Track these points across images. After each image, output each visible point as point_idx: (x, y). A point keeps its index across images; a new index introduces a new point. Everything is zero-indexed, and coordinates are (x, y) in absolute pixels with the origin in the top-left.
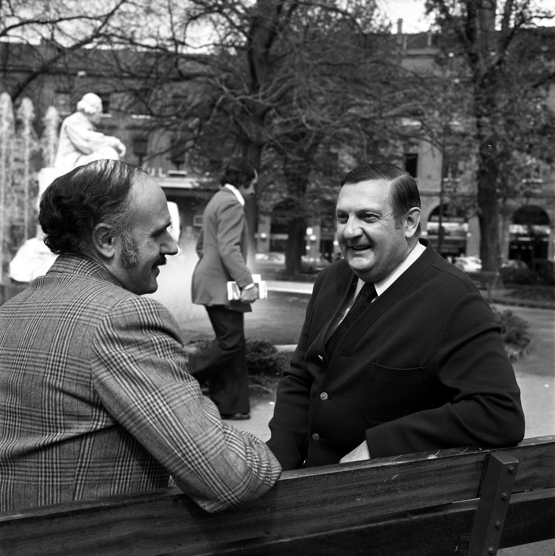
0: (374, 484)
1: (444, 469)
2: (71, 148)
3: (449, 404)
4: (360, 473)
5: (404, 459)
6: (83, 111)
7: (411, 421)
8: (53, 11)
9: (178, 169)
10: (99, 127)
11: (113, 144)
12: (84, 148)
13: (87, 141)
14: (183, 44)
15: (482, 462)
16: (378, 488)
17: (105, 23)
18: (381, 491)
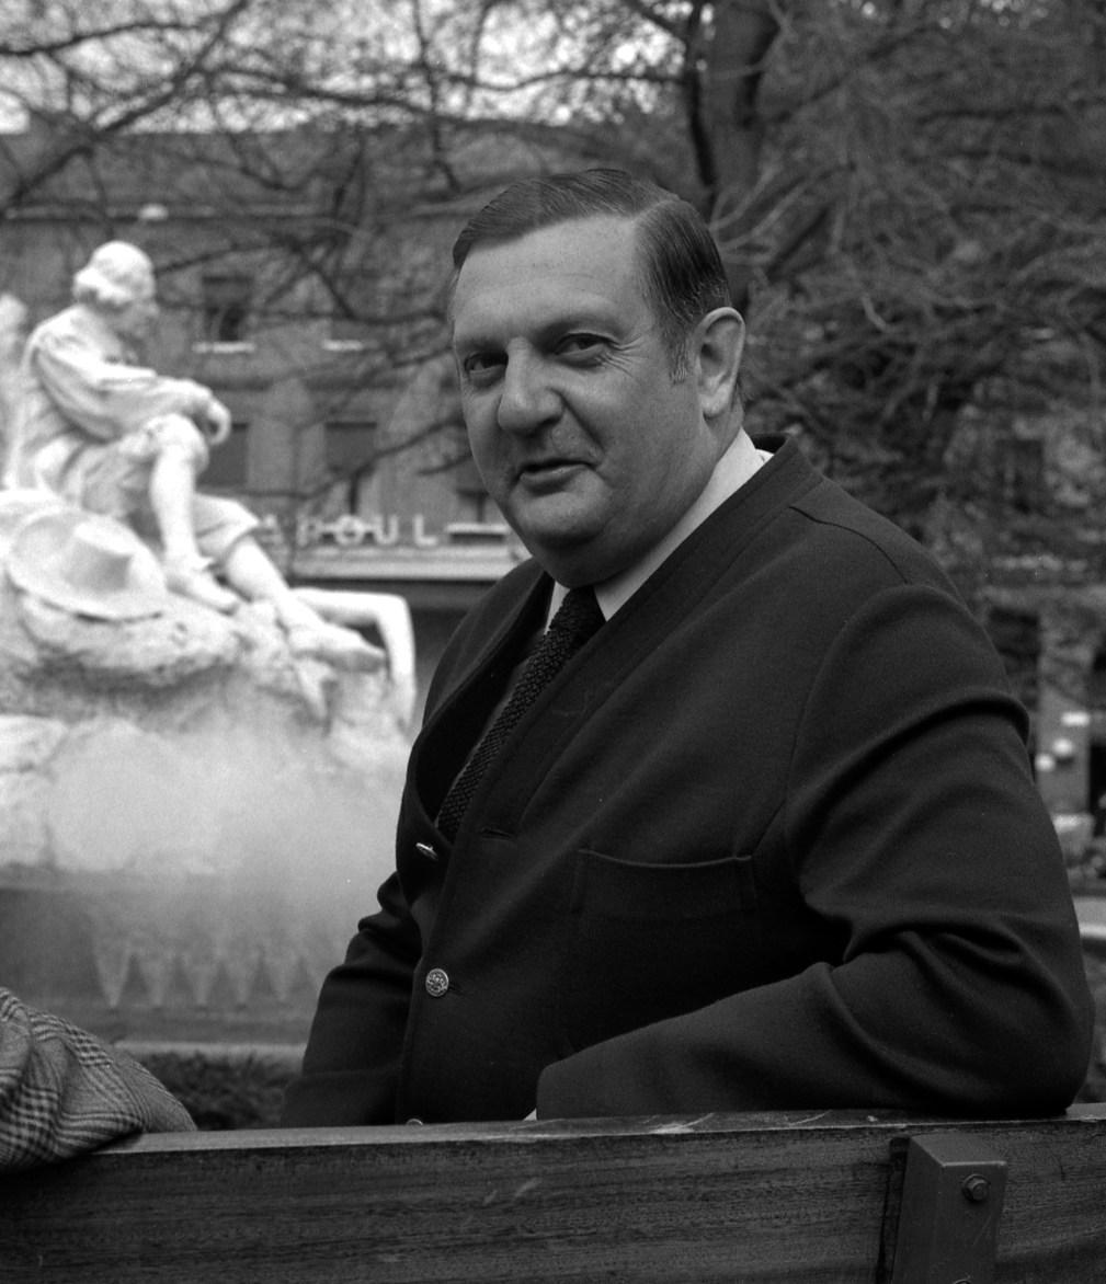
0: (444, 1207)
1: (725, 1177)
2: (48, 426)
3: (820, 969)
4: (383, 1159)
5: (564, 1127)
6: (90, 298)
7: (725, 1019)
8: (56, 13)
9: (480, 519)
10: (135, 347)
11: (186, 402)
12: (89, 416)
13: (102, 393)
14: (471, 83)
15: (883, 1167)
16: (463, 1227)
17: (221, 37)
18: (479, 1238)
